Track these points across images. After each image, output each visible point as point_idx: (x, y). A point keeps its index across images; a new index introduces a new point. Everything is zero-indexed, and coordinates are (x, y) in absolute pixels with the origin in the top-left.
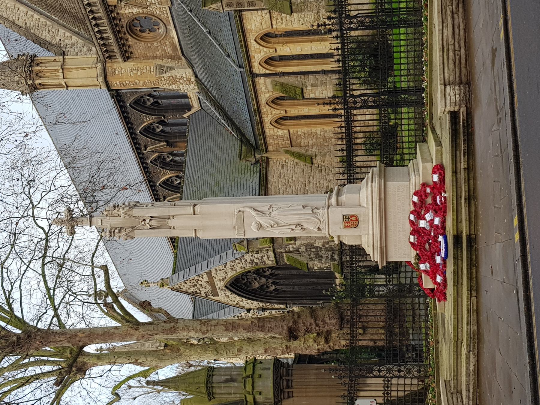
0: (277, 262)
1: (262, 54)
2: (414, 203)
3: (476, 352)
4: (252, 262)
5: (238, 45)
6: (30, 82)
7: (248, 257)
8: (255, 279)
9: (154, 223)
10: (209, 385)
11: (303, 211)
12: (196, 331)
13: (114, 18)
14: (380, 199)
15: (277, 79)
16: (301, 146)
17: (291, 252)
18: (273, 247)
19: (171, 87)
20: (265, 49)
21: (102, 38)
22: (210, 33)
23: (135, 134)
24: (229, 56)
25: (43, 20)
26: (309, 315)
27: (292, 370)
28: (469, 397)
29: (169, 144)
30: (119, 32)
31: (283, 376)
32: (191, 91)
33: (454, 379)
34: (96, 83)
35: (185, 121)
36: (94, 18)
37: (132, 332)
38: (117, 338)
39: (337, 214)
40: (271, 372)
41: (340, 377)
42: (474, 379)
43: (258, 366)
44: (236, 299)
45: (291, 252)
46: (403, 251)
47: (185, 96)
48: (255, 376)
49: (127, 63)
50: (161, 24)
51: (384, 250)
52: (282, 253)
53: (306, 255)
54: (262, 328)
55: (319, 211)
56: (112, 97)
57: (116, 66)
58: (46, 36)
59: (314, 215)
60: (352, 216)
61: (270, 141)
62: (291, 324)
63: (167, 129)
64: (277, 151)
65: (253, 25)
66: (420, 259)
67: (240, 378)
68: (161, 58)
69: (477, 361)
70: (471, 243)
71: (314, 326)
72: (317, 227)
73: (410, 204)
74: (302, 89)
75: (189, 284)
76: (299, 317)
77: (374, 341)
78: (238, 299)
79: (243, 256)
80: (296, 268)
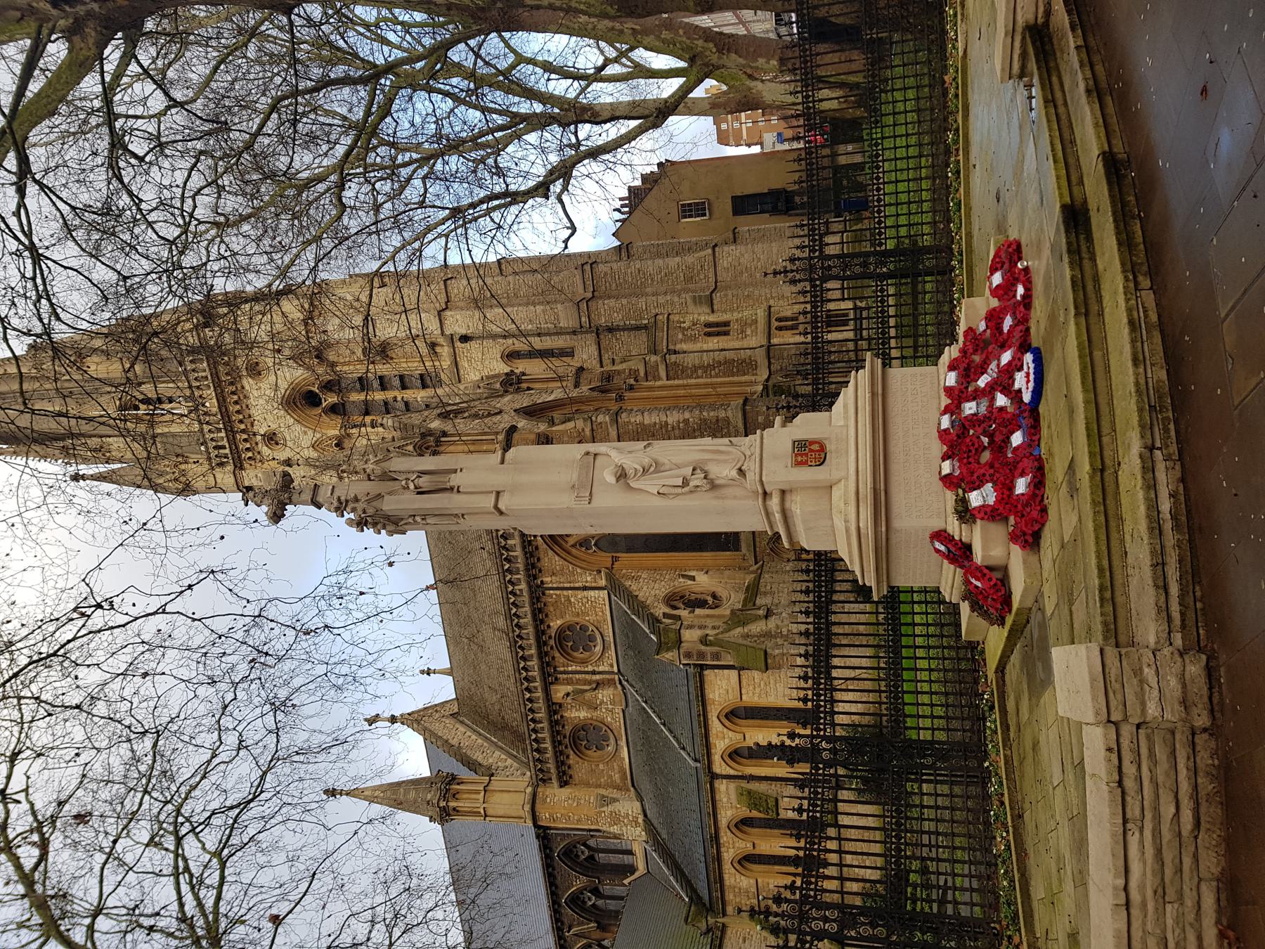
1: (727, 741)
3: (1173, 448)
5: (695, 724)
6: (443, 804)
9: (424, 482)
13: (557, 722)
14: (873, 394)
15: (744, 784)
20: (730, 733)
21: (538, 750)
22: (664, 725)
23: (560, 905)
24: (683, 749)
28: (1169, 619)
29: (602, 927)
30: (560, 743)
32: (635, 837)
33: (1102, 599)
34: (521, 813)
36: (533, 720)
41: (793, 282)
42: (1179, 545)
47: (630, 852)
49: (563, 790)
50: (612, 741)
56: (538, 837)
57: (549, 791)
58: (478, 756)
60: (812, 443)
61: (730, 896)
63: (600, 903)
68: (606, 786)
69: (1183, 480)
70: (1117, 171)
74: (777, 800)
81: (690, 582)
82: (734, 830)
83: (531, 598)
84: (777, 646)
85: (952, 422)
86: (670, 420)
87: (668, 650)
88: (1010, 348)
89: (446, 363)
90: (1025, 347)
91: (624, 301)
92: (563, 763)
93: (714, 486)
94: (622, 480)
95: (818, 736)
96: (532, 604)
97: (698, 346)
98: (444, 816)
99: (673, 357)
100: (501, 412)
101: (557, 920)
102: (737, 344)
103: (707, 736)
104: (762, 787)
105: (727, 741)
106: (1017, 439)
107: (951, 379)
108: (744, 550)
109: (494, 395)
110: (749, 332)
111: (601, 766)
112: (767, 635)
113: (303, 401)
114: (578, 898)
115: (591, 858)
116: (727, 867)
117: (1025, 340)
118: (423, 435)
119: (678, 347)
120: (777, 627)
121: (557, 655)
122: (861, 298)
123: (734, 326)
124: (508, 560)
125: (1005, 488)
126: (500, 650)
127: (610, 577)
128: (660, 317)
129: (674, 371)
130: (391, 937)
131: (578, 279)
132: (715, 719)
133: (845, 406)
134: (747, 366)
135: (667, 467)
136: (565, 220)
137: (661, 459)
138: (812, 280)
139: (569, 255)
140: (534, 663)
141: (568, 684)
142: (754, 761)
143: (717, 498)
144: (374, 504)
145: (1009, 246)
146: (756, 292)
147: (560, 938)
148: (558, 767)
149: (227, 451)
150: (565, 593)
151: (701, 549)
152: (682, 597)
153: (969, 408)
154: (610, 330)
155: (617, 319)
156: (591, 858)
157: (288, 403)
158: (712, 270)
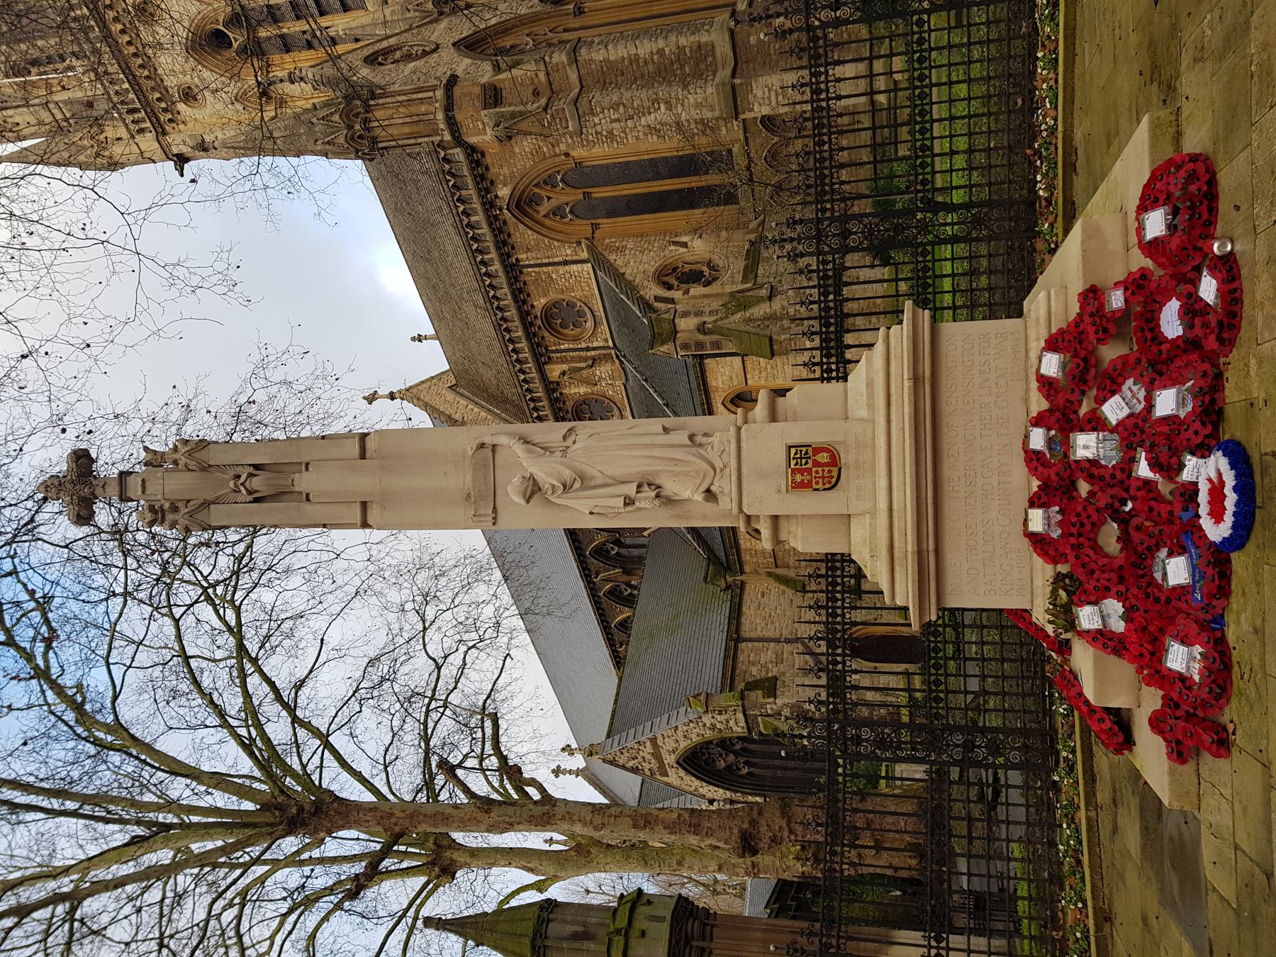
2: (1046, 384)
4: (713, 727)
7: (707, 719)
8: (721, 755)
10: (539, 943)
11: (662, 439)
12: (585, 824)
13: (557, 400)
14: (916, 379)
16: (788, 567)
18: (743, 706)
22: (667, 405)
23: (585, 556)
25: (483, 414)
26: (778, 813)
27: (713, 926)
29: (626, 572)
31: (693, 938)
35: (645, 541)
36: (532, 399)
37: (480, 815)
38: (455, 825)
39: (767, 443)
40: (665, 927)
43: (642, 910)
44: (693, 783)
46: (1001, 569)
48: (631, 932)
51: (930, 566)
52: (756, 716)
54: (695, 829)
55: (710, 439)
59: (694, 450)
60: (817, 450)
61: (746, 557)
62: (746, 826)
63: (624, 551)
64: (756, 572)
65: (720, 380)
66: (1074, 590)
67: (602, 934)
71: (786, 834)
72: (704, 488)
73: (1027, 390)
76: (760, 813)
77: (896, 869)
78: (697, 783)
81: (682, 250)
83: (508, 279)
84: (783, 329)
85: (1050, 442)
86: (641, 52)
87: (662, 344)
96: (510, 285)
100: (438, 47)
101: (584, 569)
112: (772, 317)
117: (1213, 401)
120: (783, 308)
121: (546, 334)
126: (484, 326)
127: (592, 249)
132: (719, 405)
133: (870, 384)
135: (599, 481)
140: (523, 345)
141: (563, 362)
147: (589, 583)
150: (545, 269)
151: (692, 206)
152: (675, 270)
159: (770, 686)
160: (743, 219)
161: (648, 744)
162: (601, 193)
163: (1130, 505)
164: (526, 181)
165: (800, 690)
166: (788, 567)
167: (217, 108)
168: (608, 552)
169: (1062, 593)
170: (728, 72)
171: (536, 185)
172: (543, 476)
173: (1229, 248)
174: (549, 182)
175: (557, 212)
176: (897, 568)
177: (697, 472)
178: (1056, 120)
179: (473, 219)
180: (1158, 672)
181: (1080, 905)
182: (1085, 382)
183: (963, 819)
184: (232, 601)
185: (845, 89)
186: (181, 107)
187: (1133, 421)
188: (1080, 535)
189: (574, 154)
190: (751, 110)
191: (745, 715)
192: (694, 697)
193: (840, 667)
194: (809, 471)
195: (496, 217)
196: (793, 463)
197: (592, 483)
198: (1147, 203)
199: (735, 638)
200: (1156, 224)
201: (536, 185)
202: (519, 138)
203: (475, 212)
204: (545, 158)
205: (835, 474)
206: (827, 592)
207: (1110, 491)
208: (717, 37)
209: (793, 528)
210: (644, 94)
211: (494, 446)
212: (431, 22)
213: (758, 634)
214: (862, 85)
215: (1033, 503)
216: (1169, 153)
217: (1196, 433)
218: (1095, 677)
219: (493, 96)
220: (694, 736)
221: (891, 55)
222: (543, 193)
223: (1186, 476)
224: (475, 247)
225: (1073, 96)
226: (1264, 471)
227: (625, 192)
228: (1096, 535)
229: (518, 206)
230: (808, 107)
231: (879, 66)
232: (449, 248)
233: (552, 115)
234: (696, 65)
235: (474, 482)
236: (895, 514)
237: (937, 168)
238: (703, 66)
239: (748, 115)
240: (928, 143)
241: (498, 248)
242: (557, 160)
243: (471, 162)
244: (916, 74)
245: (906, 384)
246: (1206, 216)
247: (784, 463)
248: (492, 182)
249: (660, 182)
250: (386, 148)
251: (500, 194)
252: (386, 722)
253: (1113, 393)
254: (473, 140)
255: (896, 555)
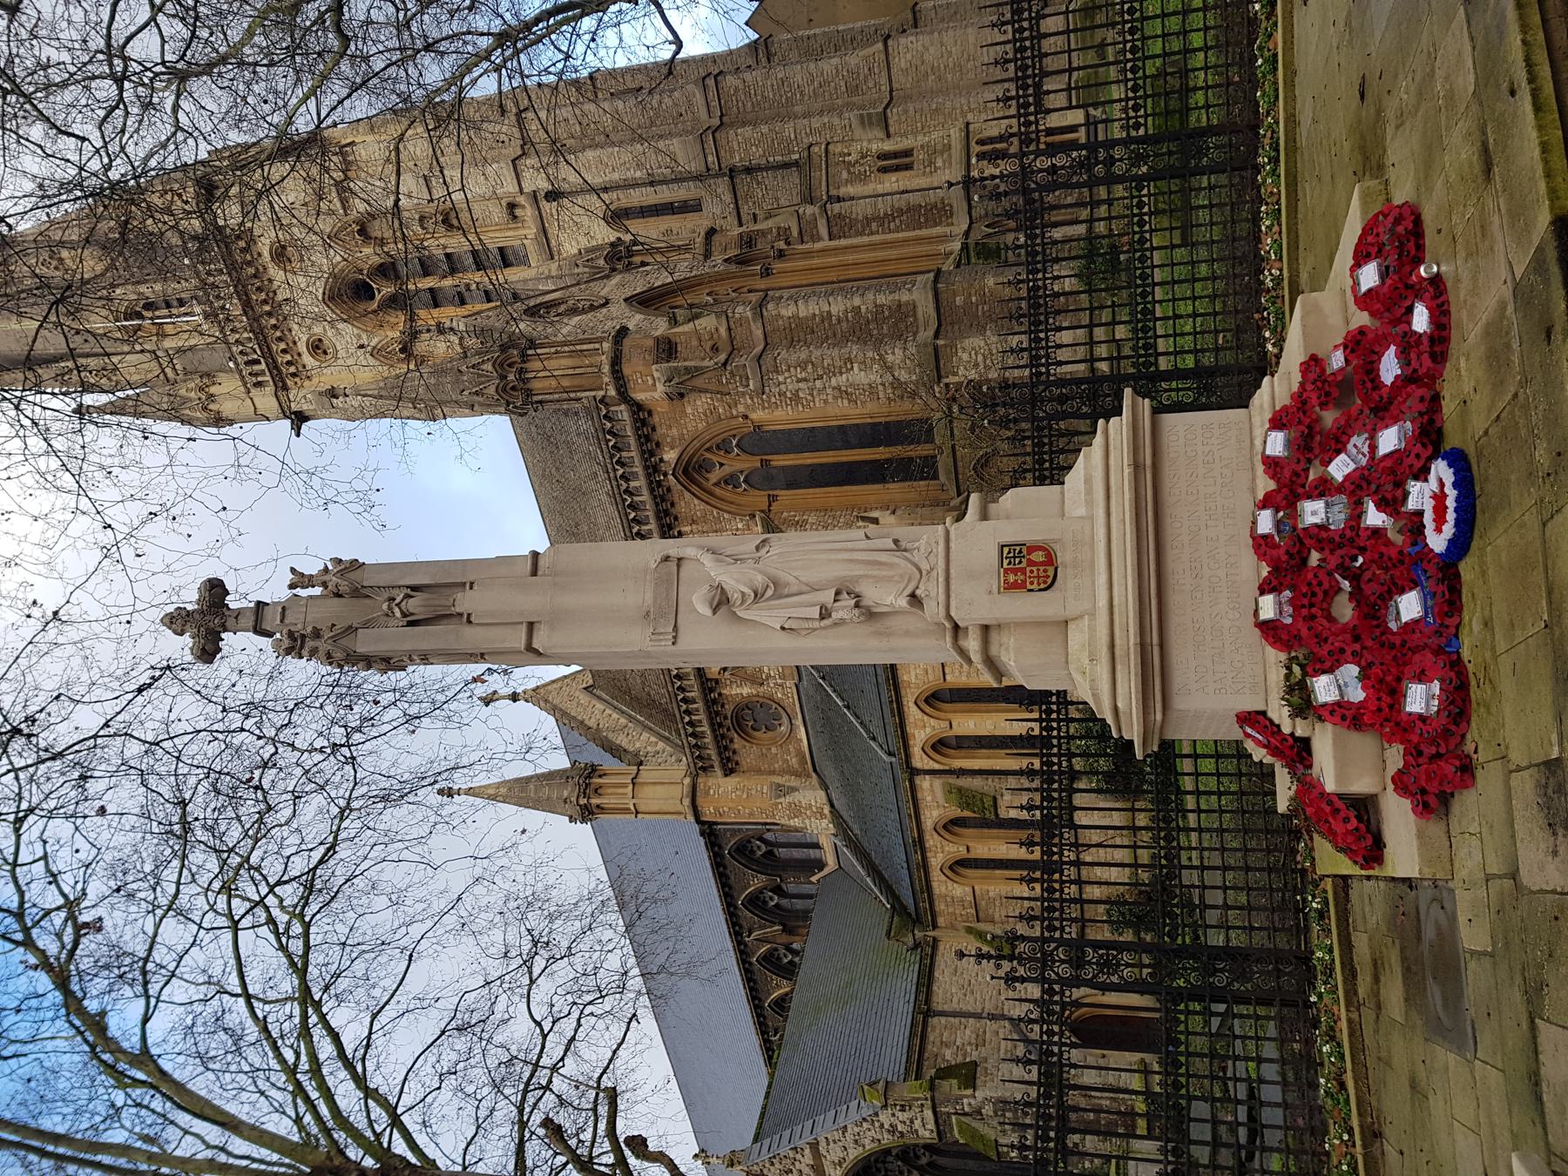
0: (939, 1133)
1: (928, 730)
2: (1272, 464)
4: (893, 1130)
6: (583, 801)
7: (885, 1117)
9: (415, 605)
11: (865, 544)
13: (714, 701)
14: (1137, 466)
15: (952, 780)
16: (993, 921)
17: (965, 1114)
18: (933, 1100)
19: (792, 823)
21: (694, 735)
22: (848, 707)
23: (736, 907)
24: (874, 739)
25: (623, 721)
29: (787, 930)
30: (720, 725)
32: (822, 830)
34: (680, 808)
36: (685, 700)
45: (965, 1114)
46: (1228, 676)
47: (817, 846)
49: (728, 779)
50: (785, 720)
52: (949, 1114)
53: (995, 1123)
56: (702, 834)
57: (711, 781)
58: (621, 740)
60: (1032, 549)
61: (940, 906)
63: (785, 902)
64: (953, 927)
68: (782, 772)
72: (908, 591)
74: (995, 799)
75: (777, 1166)
79: (876, 1114)
80: (977, 1156)
82: (943, 832)
85: (1278, 524)
88: (1395, 420)
89: (531, 230)
90: (1430, 439)
91: (765, 129)
92: (726, 748)
93: (871, 615)
94: (723, 609)
95: (1051, 939)
97: (869, 188)
98: (586, 814)
99: (836, 206)
100: (607, 302)
101: (734, 924)
102: (923, 182)
103: (902, 725)
104: (976, 783)
105: (928, 730)
106: (1409, 606)
107: (1276, 444)
108: (942, 478)
109: (599, 276)
110: (939, 163)
111: (774, 750)
113: (351, 293)
114: (758, 898)
115: (770, 853)
116: (937, 877)
117: (1431, 421)
118: (504, 348)
119: (843, 191)
122: (1095, 105)
123: (920, 156)
124: (633, 506)
125: (1386, 690)
128: (815, 149)
129: (839, 227)
130: (531, 973)
131: (699, 98)
132: (911, 704)
133: (1088, 481)
134: (937, 213)
135: (794, 589)
136: (665, 30)
137: (784, 576)
138: (1025, 192)
139: (684, 61)
142: (963, 752)
143: (878, 634)
144: (344, 642)
145: (1397, 221)
146: (948, 104)
147: (739, 943)
148: (720, 754)
149: (263, 366)
151: (882, 480)
153: (1313, 512)
154: (748, 170)
155: (757, 155)
156: (770, 853)
157: (331, 298)
158: (884, 74)
159: (968, 1074)
160: (944, 496)
161: (807, 1151)
162: (780, 461)
163: (1361, 560)
164: (696, 444)
165: (1006, 1080)
166: (993, 921)
167: (353, 351)
168: (765, 902)
169: (1296, 669)
170: (931, 333)
171: (708, 450)
172: (732, 582)
173: (1435, 269)
174: (723, 446)
175: (730, 480)
176: (1119, 667)
177: (901, 576)
178: (1281, 270)
179: (632, 484)
180: (1397, 724)
181: (1346, 1137)
182: (1310, 450)
183: (1205, 1055)
184: (302, 915)
185: (1062, 355)
186: (308, 359)
187: (1358, 474)
188: (1312, 605)
189: (753, 416)
190: (955, 374)
191: (935, 1113)
192: (870, 1085)
193: (1056, 857)
194: (1023, 571)
195: (659, 483)
196: (1006, 562)
197: (786, 591)
198: (1360, 258)
199: (924, 1011)
200: (1369, 276)
201: (708, 450)
202: (692, 396)
203: (635, 476)
204: (720, 419)
205: (1051, 573)
206: (1043, 900)
207: (1340, 552)
208: (919, 296)
209: (1004, 640)
210: (836, 352)
211: (679, 559)
212: (602, 278)
213: (954, 1006)
214: (1081, 352)
215: (1264, 589)
216: (1377, 208)
217: (1418, 456)
218: (1335, 757)
219: (667, 349)
220: (867, 1142)
221: (1114, 323)
222: (715, 459)
223: (1412, 504)
224: (632, 515)
225: (1297, 243)
226: (1480, 455)
227: (809, 461)
228: (1329, 605)
229: (685, 472)
230: (1027, 372)
231: (1099, 333)
232: (601, 520)
233: (731, 373)
234: (899, 322)
235: (655, 598)
236: (1116, 610)
237: (1160, 332)
238: (903, 326)
239: (952, 379)
240: (1152, 359)
241: (659, 518)
242: (733, 422)
243: (636, 421)
244: (1141, 343)
245: (1126, 471)
246: (1413, 252)
247: (996, 562)
248: (658, 444)
249: (849, 452)
250: (540, 402)
251: (666, 457)
252: (470, 1110)
253: (1338, 453)
254: (640, 396)
255: (1118, 652)
